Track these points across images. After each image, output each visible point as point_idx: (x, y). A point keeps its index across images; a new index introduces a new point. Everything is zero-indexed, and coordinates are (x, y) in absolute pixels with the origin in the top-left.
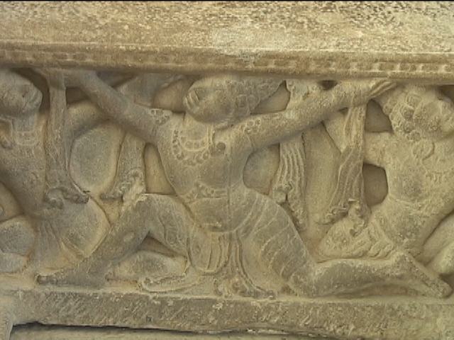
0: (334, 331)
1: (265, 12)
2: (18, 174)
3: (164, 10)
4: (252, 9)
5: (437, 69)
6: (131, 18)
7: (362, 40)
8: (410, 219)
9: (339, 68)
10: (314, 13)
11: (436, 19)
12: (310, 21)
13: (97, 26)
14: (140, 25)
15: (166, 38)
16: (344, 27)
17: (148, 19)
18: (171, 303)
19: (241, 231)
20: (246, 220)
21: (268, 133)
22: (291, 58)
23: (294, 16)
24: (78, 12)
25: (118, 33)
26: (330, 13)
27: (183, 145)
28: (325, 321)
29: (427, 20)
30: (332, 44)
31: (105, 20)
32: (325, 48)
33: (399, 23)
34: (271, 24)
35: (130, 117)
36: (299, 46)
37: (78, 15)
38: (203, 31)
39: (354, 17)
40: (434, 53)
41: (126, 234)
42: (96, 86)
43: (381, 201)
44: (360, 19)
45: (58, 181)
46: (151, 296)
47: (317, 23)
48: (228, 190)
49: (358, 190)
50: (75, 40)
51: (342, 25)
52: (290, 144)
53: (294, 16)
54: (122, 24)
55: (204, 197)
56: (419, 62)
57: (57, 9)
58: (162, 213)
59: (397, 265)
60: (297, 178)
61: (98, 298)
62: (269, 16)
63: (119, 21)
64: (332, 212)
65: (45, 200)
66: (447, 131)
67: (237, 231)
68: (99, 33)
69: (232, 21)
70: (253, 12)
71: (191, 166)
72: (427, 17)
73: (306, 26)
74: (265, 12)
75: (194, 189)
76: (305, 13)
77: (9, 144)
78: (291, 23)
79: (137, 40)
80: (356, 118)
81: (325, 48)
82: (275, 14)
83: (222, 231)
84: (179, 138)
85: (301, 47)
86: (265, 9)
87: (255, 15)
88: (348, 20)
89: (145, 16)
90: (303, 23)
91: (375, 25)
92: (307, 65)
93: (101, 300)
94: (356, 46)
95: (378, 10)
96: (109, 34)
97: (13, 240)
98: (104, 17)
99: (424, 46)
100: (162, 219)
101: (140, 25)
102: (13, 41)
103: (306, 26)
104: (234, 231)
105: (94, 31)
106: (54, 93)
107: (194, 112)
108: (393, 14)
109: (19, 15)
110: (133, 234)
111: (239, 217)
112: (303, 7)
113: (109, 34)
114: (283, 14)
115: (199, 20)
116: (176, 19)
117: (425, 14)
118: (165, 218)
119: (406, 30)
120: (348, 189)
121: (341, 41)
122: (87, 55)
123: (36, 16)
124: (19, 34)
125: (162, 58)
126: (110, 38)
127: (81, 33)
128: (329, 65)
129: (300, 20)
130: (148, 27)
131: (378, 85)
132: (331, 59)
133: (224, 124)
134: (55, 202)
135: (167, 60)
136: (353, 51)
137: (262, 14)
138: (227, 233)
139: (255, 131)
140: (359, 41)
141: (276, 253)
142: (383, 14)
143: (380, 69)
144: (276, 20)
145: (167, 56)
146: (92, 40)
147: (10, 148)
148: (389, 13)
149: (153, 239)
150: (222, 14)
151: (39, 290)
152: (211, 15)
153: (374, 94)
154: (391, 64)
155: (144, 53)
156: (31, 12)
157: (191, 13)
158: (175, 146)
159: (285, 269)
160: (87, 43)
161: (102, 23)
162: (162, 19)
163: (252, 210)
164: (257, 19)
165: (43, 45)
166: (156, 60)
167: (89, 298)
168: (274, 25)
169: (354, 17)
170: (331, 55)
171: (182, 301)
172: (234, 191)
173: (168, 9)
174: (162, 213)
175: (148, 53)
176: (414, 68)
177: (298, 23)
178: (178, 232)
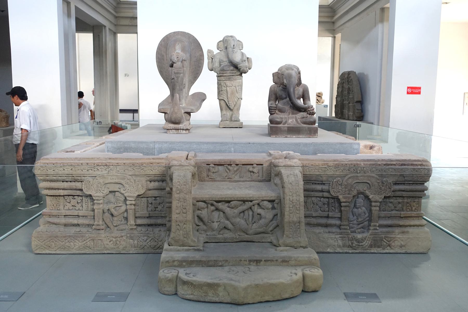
42: (215, 203)
80: (256, 206)
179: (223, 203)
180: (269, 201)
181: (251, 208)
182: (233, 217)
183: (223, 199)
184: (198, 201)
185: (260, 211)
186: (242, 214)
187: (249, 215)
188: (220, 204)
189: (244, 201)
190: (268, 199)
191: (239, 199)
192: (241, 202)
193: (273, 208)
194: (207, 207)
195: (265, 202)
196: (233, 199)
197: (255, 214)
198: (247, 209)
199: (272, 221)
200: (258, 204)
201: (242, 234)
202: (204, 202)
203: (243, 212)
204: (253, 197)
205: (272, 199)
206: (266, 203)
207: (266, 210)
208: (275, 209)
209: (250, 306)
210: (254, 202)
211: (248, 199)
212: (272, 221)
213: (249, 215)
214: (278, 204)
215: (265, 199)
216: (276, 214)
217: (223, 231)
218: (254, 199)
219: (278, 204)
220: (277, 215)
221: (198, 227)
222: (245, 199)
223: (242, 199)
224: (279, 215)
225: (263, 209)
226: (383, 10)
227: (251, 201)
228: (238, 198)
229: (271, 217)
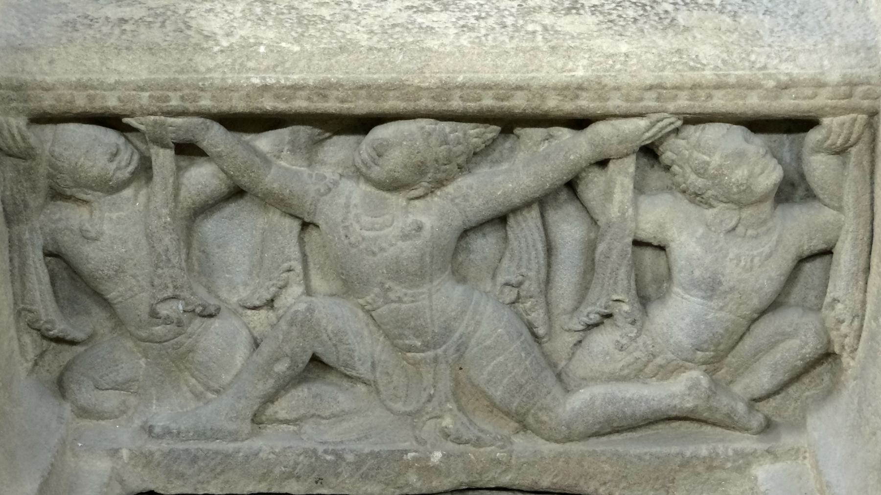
0: (596, 490)
1: (477, 18)
2: (109, 278)
3: (322, 19)
4: (458, 14)
5: (744, 98)
6: (271, 34)
7: (626, 55)
8: (706, 324)
9: (593, 100)
10: (551, 17)
11: (737, 19)
12: (545, 28)
13: (216, 49)
14: (283, 44)
15: (324, 64)
16: (598, 36)
17: (296, 35)
18: (350, 458)
19: (451, 351)
20: (457, 335)
21: (487, 203)
22: (519, 88)
23: (521, 22)
24: (189, 27)
25: (248, 59)
26: (577, 17)
27: (357, 227)
28: (581, 477)
29: (724, 21)
30: (580, 64)
31: (230, 38)
32: (570, 71)
33: (682, 28)
34: (486, 35)
35: (275, 185)
36: (530, 68)
37: (189, 33)
38: (379, 50)
39: (611, 21)
40: (740, 73)
41: (278, 360)
42: (215, 137)
43: (662, 296)
44: (621, 23)
45: (170, 285)
46: (321, 449)
47: (556, 32)
48: (429, 290)
49: (625, 282)
50: (182, 72)
51: (595, 34)
52: (115, 301)
53: (521, 22)
54: (255, 44)
55: (392, 301)
56: (718, 87)
57: (158, 25)
58: (330, 328)
59: (687, 392)
60: (534, 266)
61: (241, 454)
62: (482, 23)
63: (252, 41)
64: (588, 316)
65: (154, 314)
66: (759, 190)
67: (445, 351)
68: (220, 59)
69: (426, 32)
70: (459, 19)
71: (370, 257)
72: (724, 17)
73: (539, 38)
74: (477, 18)
75: (377, 290)
76: (538, 17)
77: (93, 234)
78: (517, 34)
79: (279, 69)
80: (623, 174)
81: (570, 71)
82: (493, 19)
83: (423, 351)
84: (351, 216)
85: (533, 71)
86: (477, 14)
87: (461, 23)
88: (604, 26)
89: (292, 30)
90: (534, 32)
91: (646, 31)
92: (543, 98)
93: (247, 457)
94: (618, 66)
95: (648, 8)
96: (235, 60)
97: (111, 372)
98: (228, 35)
99: (724, 61)
100: (331, 335)
101: (283, 44)
102: (85, 78)
103: (539, 38)
104: (440, 351)
105: (213, 57)
106: (157, 155)
107: (373, 175)
108: (673, 14)
109: (98, 36)
110: (288, 360)
111: (447, 331)
112: (534, 8)
113: (235, 60)
114: (505, 20)
115: (376, 34)
116: (340, 34)
117: (721, 12)
118: (336, 335)
119: (694, 37)
120: (611, 282)
121: (596, 59)
122: (201, 94)
123: (124, 37)
124: (94, 65)
125: (319, 95)
126: (237, 67)
127: (191, 60)
128: (577, 97)
129: (530, 27)
130: (296, 48)
131: (653, 125)
132: (580, 88)
133: (419, 192)
134: (168, 317)
135: (325, 97)
136: (613, 74)
137: (473, 21)
138: (430, 354)
139: (466, 201)
140: (623, 59)
141: (505, 381)
142: (657, 14)
143: (658, 99)
144: (493, 29)
145: (328, 93)
146: (209, 70)
147: (96, 239)
148: (666, 12)
149: (322, 362)
150: (411, 23)
151: (152, 446)
152: (394, 26)
153: (649, 138)
154: (675, 92)
155: (289, 88)
156: (117, 31)
157: (363, 22)
158: (346, 228)
159: (519, 404)
160: (201, 76)
161: (225, 43)
162: (318, 34)
163: (467, 318)
164: (465, 29)
165: (131, 82)
166: (309, 99)
167: (227, 456)
168: (490, 38)
169: (611, 21)
170: (580, 81)
171: (367, 455)
172: (438, 290)
173: (328, 18)
174: (330, 328)
175: (296, 88)
176: (709, 97)
177: (527, 33)
178: (356, 354)
179: (304, 132)
180: (758, 125)
181: (572, 186)
182: (399, 273)
183: (300, 104)
184: (43, 119)
185: (659, 215)
186: (485, 245)
187: (549, 250)
188: (264, 142)
189: (509, 123)
190: (754, 103)
191: (456, 104)
192: (475, 134)
193: (792, 190)
194: (145, 170)
195: (713, 132)
196: (391, 104)
197: (615, 248)
198: (542, 202)
199: (774, 305)
200: (650, 152)
201: (489, 425)
202: (112, 121)
203: (501, 220)
204: (601, 90)
205: (787, 105)
206: (720, 144)
207: (721, 215)
208: (810, 195)
209: (865, 254)
210: (601, 129)
211: (552, 104)
212: (774, 305)
213: (549, 250)
214: (841, 152)
215: (719, 103)
216: (818, 245)
217: (302, 392)
218: (615, 103)
219: (841, 152)
220: (828, 252)
221: (68, 353)
222: (519, 103)
223: (488, 102)
224: (846, 256)
225: (697, 198)
226: (671, 189)
227: (579, 123)
228: (445, 89)
229: (767, 278)
